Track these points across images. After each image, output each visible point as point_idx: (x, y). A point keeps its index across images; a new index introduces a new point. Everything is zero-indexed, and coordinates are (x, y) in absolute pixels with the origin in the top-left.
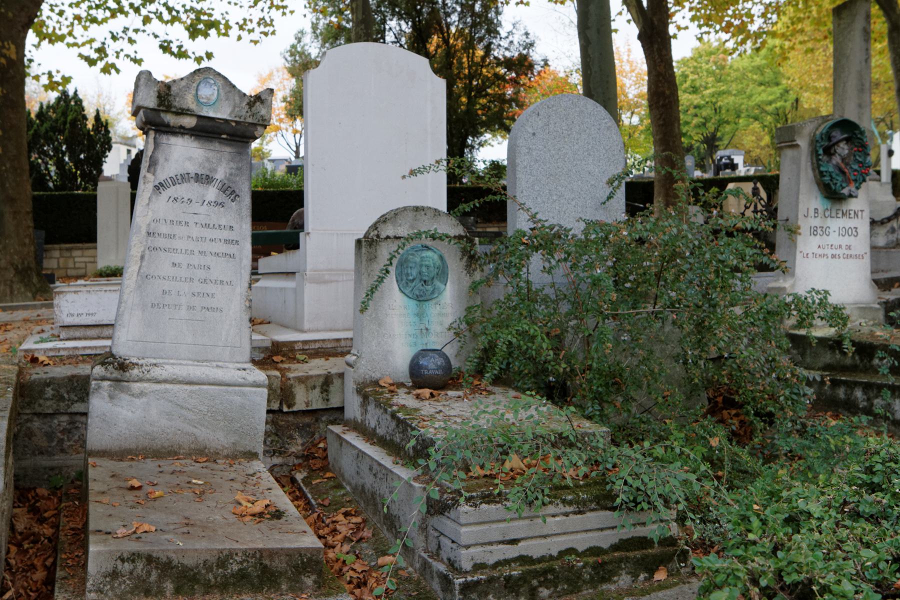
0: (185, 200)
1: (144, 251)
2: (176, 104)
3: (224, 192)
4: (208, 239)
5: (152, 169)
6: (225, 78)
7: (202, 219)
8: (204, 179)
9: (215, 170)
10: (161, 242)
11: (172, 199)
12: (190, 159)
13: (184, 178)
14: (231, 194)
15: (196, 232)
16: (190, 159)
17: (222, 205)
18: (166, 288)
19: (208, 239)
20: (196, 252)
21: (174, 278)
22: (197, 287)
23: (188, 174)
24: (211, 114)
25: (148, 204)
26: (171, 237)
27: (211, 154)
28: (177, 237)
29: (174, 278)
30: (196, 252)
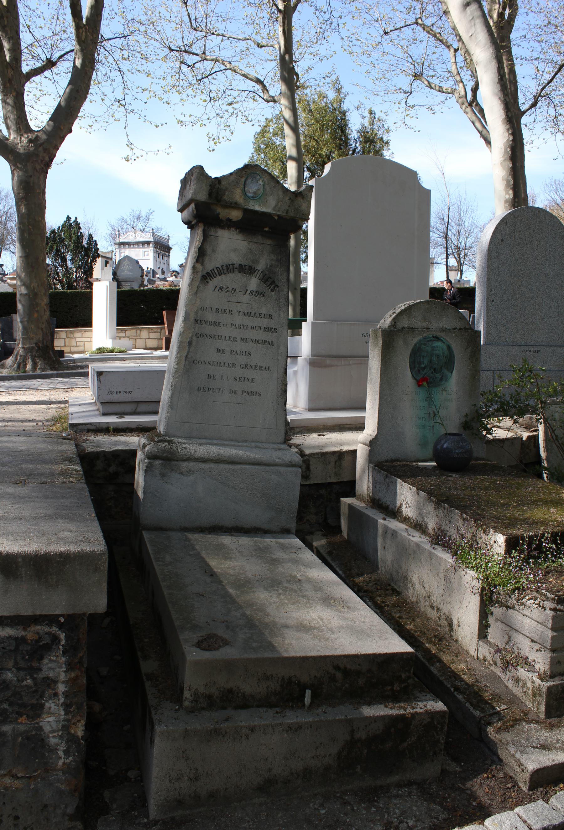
1: (192, 338)
3: (265, 282)
4: (249, 327)
5: (201, 260)
8: (246, 270)
10: (208, 329)
11: (218, 288)
12: (235, 250)
13: (228, 269)
14: (271, 284)
15: (238, 319)
16: (235, 250)
17: (263, 294)
19: (249, 327)
20: (239, 339)
21: (219, 364)
23: (233, 264)
24: (257, 208)
25: (196, 293)
26: (216, 324)
29: (219, 364)
30: (239, 339)
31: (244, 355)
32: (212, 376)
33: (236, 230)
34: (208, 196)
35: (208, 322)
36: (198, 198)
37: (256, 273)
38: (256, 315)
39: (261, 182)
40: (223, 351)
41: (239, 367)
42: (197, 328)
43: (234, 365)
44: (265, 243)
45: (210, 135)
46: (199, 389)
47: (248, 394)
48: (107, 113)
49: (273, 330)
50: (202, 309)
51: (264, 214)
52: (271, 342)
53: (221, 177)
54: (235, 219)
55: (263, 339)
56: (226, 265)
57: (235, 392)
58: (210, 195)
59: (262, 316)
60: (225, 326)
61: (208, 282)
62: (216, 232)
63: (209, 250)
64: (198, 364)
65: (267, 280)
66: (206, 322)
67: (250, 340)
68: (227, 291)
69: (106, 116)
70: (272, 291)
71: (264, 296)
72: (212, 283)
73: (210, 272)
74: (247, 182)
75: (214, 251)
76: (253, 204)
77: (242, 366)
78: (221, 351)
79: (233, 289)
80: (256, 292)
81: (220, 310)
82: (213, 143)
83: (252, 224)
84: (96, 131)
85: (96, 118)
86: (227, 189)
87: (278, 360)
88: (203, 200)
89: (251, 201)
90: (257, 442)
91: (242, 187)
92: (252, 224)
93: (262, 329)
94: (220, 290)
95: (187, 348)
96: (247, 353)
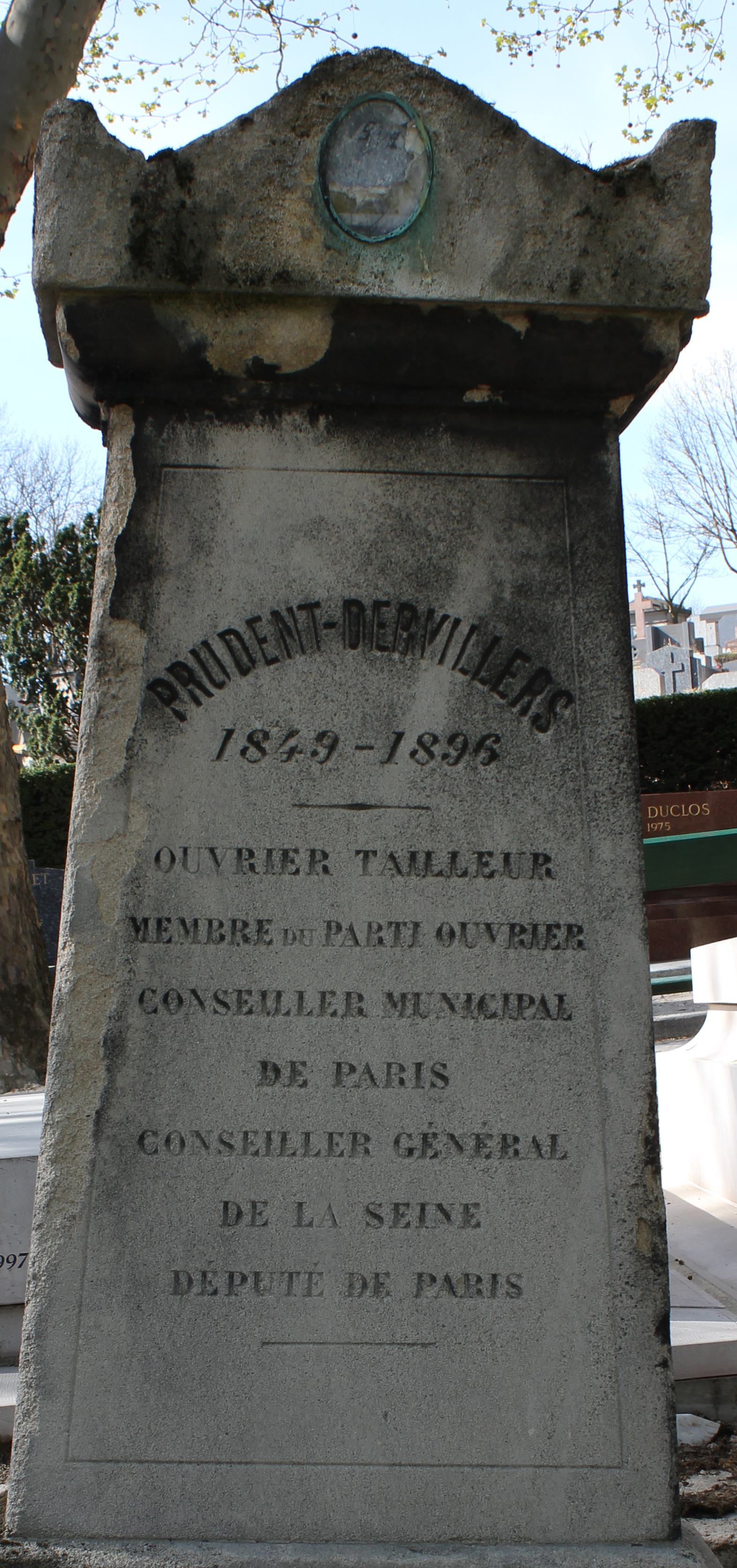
0: (306, 736)
1: (119, 1017)
2: (224, 253)
3: (494, 683)
4: (428, 930)
5: (135, 602)
6: (461, 92)
7: (386, 831)
8: (388, 626)
9: (442, 576)
10: (203, 965)
11: (239, 741)
12: (315, 529)
13: (289, 630)
14: (530, 690)
15: (365, 898)
16: (315, 529)
17: (486, 748)
18: (240, 1193)
19: (428, 930)
20: (374, 1003)
21: (278, 1142)
22: (392, 1178)
23: (310, 607)
24: (405, 286)
25: (125, 778)
26: (246, 931)
27: (417, 495)
28: (274, 933)
29: (278, 1142)
30: (374, 1003)
31: (410, 1083)
32: (246, 1208)
33: (313, 420)
34: (126, 257)
35: (203, 927)
36: (75, 278)
37: (441, 638)
38: (462, 862)
39: (412, 143)
40: (295, 1072)
41: (390, 1150)
42: (142, 963)
43: (359, 1141)
44: (476, 469)
45: (630, 77)
46: (180, 1284)
47: (452, 1291)
48: (206, 46)
49: (561, 934)
50: (165, 859)
51: (449, 314)
52: (553, 1003)
53: (192, 145)
54: (291, 364)
55: (513, 988)
56: (275, 614)
57: (379, 1285)
58: (138, 248)
59: (496, 863)
60: (292, 936)
61: (182, 717)
62: (203, 442)
63: (173, 544)
64: (163, 1155)
65: (507, 670)
66: (189, 927)
67: (436, 1004)
68: (292, 751)
69: (201, 55)
70: (539, 724)
71: (493, 756)
72: (205, 720)
73: (192, 662)
74: (338, 154)
75: (200, 547)
76: (378, 265)
77: (404, 1143)
78: (286, 1072)
79: (321, 736)
80: (451, 740)
81: (260, 856)
82: (642, 104)
83: (392, 377)
84: (170, 121)
85: (165, 73)
86: (226, 205)
87: (603, 1094)
88: (104, 283)
89: (367, 253)
90: (520, 1541)
91: (313, 180)
92: (392, 377)
93: (502, 936)
94: (253, 752)
95: (102, 1073)
96: (426, 1074)
